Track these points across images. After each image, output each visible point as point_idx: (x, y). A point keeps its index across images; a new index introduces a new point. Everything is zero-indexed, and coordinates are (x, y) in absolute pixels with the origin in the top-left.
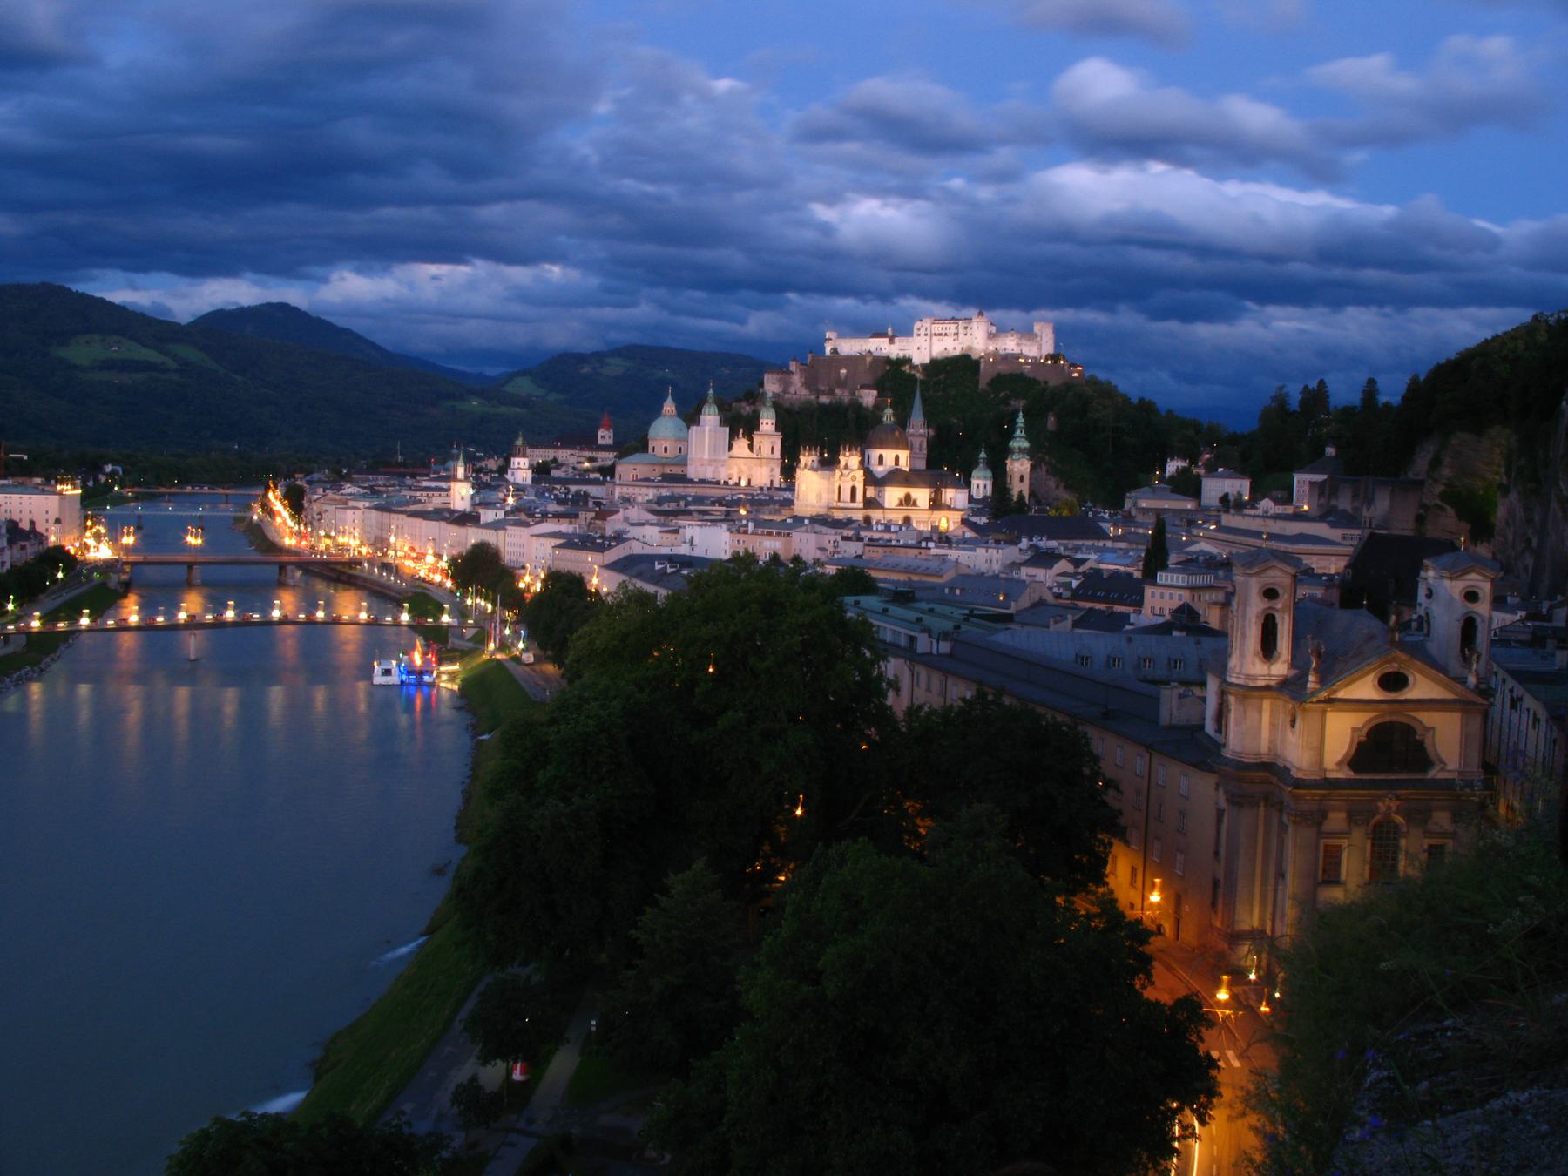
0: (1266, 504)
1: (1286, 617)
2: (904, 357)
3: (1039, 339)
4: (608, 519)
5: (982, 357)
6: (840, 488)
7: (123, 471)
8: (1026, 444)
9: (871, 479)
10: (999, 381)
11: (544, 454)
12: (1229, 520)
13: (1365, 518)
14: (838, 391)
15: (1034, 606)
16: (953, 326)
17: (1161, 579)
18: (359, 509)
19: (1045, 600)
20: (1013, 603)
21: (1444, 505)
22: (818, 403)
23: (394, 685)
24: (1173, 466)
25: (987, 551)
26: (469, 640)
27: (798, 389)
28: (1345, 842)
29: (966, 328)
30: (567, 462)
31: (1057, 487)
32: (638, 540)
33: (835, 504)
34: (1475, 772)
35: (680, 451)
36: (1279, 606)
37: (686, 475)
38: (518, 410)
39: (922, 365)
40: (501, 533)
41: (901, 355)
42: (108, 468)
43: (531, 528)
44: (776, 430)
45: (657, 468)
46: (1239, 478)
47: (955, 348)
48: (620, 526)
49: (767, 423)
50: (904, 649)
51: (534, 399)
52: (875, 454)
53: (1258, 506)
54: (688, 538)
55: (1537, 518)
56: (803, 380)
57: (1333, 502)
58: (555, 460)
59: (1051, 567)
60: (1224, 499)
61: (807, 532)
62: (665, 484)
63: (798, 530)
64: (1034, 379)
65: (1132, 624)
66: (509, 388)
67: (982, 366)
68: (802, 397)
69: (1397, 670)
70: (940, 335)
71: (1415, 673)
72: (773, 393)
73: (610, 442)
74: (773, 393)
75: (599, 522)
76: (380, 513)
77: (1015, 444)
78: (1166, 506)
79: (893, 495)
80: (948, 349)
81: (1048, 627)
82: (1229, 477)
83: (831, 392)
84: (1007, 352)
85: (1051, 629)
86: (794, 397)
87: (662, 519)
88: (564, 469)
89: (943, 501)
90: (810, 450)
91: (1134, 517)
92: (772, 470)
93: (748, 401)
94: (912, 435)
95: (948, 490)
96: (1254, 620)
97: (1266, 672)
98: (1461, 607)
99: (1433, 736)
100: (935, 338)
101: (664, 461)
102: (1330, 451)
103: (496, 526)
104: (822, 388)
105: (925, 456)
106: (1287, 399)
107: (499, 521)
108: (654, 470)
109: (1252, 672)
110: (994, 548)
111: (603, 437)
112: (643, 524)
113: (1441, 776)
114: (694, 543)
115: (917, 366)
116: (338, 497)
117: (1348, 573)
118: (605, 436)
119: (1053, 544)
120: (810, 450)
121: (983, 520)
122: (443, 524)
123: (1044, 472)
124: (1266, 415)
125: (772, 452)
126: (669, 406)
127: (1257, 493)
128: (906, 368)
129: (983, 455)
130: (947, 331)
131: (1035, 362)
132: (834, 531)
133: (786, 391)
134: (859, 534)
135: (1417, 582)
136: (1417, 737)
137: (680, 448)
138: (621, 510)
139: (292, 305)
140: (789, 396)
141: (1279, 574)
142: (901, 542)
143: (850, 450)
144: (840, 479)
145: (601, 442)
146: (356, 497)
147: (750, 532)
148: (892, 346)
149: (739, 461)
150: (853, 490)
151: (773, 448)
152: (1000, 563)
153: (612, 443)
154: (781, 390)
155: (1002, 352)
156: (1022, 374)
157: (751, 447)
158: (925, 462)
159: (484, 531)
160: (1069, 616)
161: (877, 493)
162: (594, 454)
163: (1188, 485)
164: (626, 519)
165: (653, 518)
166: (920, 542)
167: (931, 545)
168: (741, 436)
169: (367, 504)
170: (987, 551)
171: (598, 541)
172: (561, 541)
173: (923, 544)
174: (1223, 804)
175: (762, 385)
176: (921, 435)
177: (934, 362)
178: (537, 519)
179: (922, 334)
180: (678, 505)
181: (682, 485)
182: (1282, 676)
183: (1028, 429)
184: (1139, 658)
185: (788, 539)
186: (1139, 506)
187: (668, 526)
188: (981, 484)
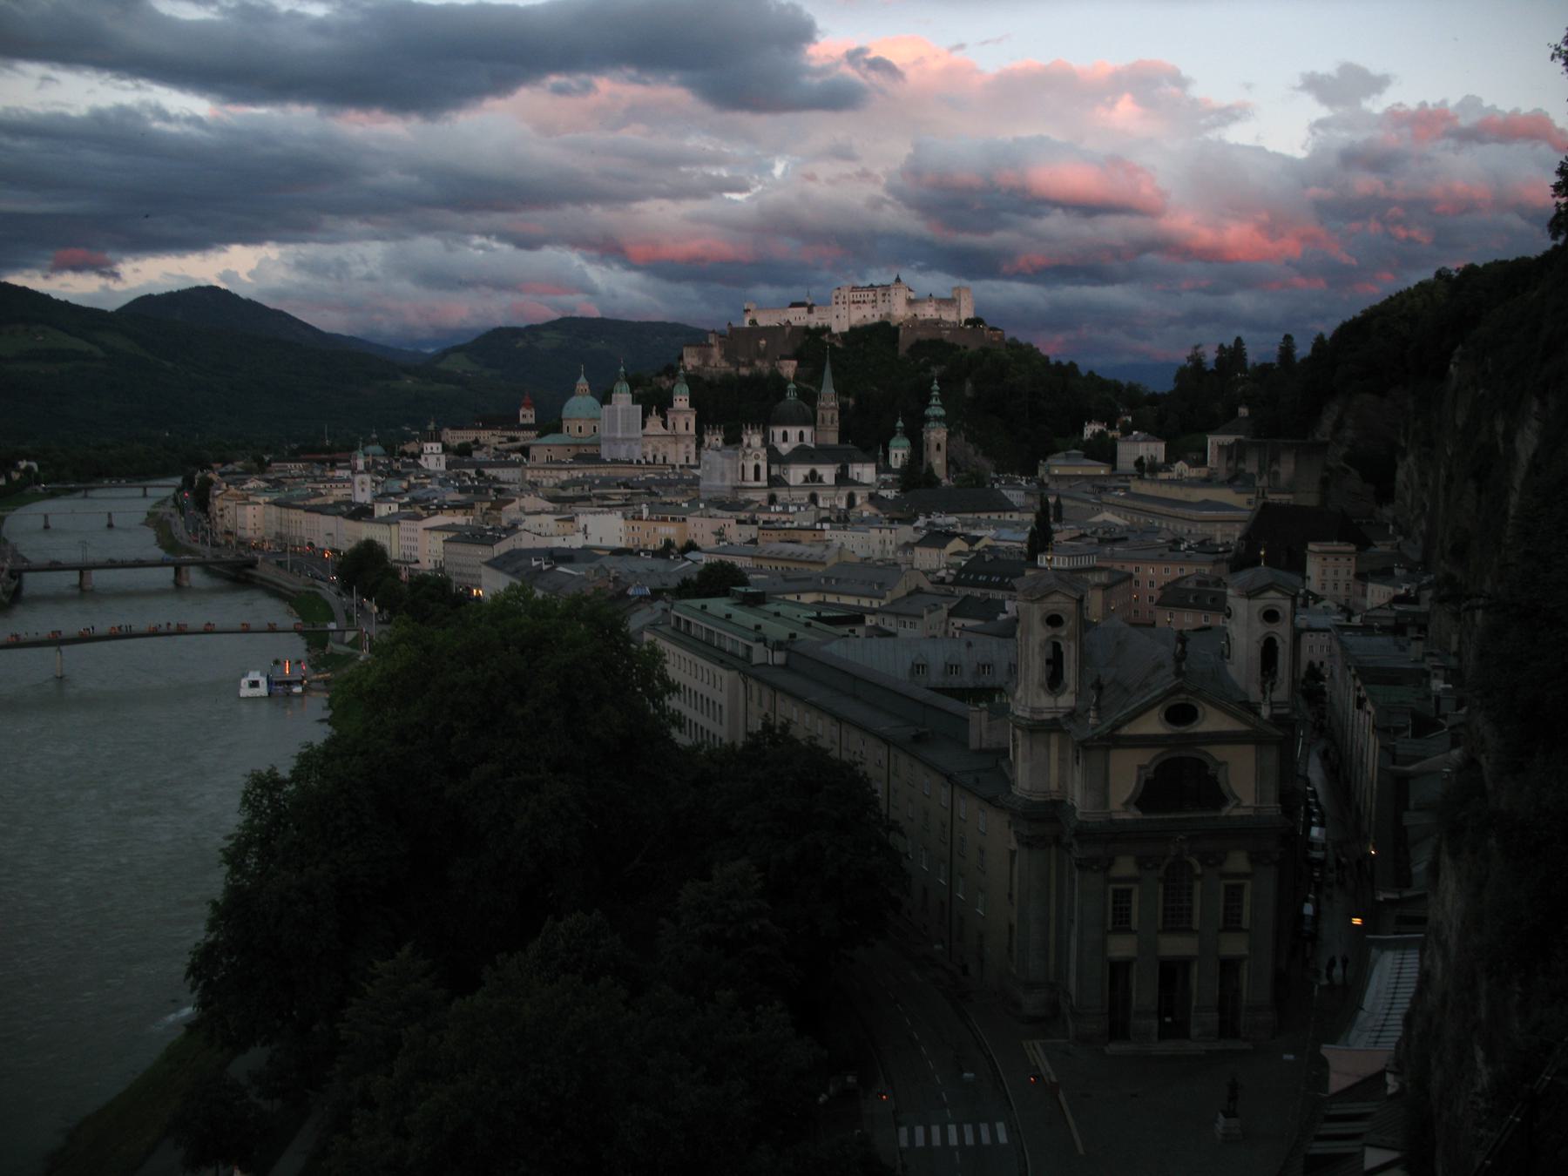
0: (1180, 466)
1: (1072, 644)
2: (823, 326)
3: (957, 304)
4: (504, 508)
5: (901, 324)
6: (743, 466)
7: (39, 467)
8: (942, 412)
9: (774, 456)
10: (918, 347)
11: (465, 436)
12: (1137, 486)
13: (1258, 487)
14: (758, 363)
15: (910, 594)
16: (871, 294)
17: (1041, 562)
18: (258, 504)
19: (922, 588)
20: (888, 593)
21: (1348, 467)
22: (738, 375)
23: (261, 697)
24: (1090, 430)
25: (880, 532)
26: (348, 644)
27: (718, 363)
29: (884, 295)
30: (488, 443)
31: (976, 453)
32: (529, 531)
33: (739, 484)
34: (1272, 808)
35: (595, 431)
36: (1064, 633)
37: (600, 455)
38: (453, 387)
39: (841, 333)
40: (394, 528)
41: (820, 324)
42: (23, 464)
43: (424, 521)
44: (690, 406)
45: (572, 449)
46: (1154, 441)
47: (874, 316)
48: (514, 516)
49: (682, 401)
50: (742, 659)
51: (470, 375)
52: (778, 431)
53: (1172, 469)
54: (581, 526)
55: (1430, 483)
56: (723, 352)
57: (1241, 466)
58: (476, 441)
59: (944, 546)
60: (1139, 463)
61: (702, 516)
62: (576, 466)
63: (692, 514)
64: (954, 345)
65: (1006, 612)
66: (443, 366)
67: (901, 332)
68: (722, 369)
69: (1184, 702)
70: (859, 302)
72: (693, 366)
73: (532, 420)
74: (693, 366)
75: (494, 512)
76: (278, 509)
77: (930, 413)
78: (1080, 473)
79: (797, 474)
80: (867, 316)
81: (922, 617)
82: (1144, 440)
83: (751, 364)
84: (926, 317)
85: (925, 618)
86: (714, 370)
87: (558, 506)
88: (485, 449)
89: (850, 476)
90: (714, 428)
91: (1047, 485)
92: (687, 446)
93: (668, 375)
94: (823, 408)
95: (855, 465)
96: (1037, 649)
97: (1053, 705)
98: (1261, 629)
100: (853, 306)
101: (578, 441)
102: (1243, 411)
103: (388, 521)
104: (742, 360)
105: (838, 429)
106: (1202, 358)
107: (393, 514)
108: (569, 450)
109: (1037, 705)
110: (887, 528)
111: (524, 416)
112: (538, 513)
113: (1236, 812)
114: (589, 530)
115: (836, 335)
116: (239, 493)
117: (1242, 545)
118: (527, 416)
119: (952, 519)
120: (714, 428)
121: (890, 494)
122: (340, 519)
123: (963, 439)
124: (1182, 374)
125: (687, 428)
126: (582, 383)
127: (1173, 456)
128: (826, 337)
129: (900, 424)
130: (866, 299)
131: (956, 328)
132: (729, 514)
133: (705, 363)
134: (754, 516)
135: (1305, 556)
136: (1209, 772)
137: (595, 428)
138: (517, 499)
139: (155, 294)
140: (709, 369)
141: (1062, 599)
142: (795, 525)
143: (752, 429)
144: (743, 458)
145: (522, 421)
146: (257, 491)
147: (644, 518)
148: (811, 316)
149: (653, 439)
150: (757, 468)
151: (687, 425)
152: (894, 543)
153: (534, 422)
154: (701, 363)
155: (921, 318)
156: (942, 340)
157: (665, 426)
158: (837, 434)
159: (379, 526)
160: (945, 606)
161: (782, 470)
162: (517, 434)
163: (1103, 451)
164: (522, 509)
165: (549, 506)
166: (815, 524)
167: (826, 526)
168: (654, 413)
169: (267, 499)
170: (880, 532)
171: (488, 533)
172: (451, 535)
173: (818, 526)
174: (1014, 845)
175: (681, 358)
176: (832, 408)
177: (853, 329)
178: (432, 512)
179: (840, 303)
180: (583, 489)
181: (594, 466)
182: (1069, 707)
183: (943, 396)
184: (978, 664)
185: (682, 524)
186: (1052, 473)
187: (564, 514)
188: (898, 453)
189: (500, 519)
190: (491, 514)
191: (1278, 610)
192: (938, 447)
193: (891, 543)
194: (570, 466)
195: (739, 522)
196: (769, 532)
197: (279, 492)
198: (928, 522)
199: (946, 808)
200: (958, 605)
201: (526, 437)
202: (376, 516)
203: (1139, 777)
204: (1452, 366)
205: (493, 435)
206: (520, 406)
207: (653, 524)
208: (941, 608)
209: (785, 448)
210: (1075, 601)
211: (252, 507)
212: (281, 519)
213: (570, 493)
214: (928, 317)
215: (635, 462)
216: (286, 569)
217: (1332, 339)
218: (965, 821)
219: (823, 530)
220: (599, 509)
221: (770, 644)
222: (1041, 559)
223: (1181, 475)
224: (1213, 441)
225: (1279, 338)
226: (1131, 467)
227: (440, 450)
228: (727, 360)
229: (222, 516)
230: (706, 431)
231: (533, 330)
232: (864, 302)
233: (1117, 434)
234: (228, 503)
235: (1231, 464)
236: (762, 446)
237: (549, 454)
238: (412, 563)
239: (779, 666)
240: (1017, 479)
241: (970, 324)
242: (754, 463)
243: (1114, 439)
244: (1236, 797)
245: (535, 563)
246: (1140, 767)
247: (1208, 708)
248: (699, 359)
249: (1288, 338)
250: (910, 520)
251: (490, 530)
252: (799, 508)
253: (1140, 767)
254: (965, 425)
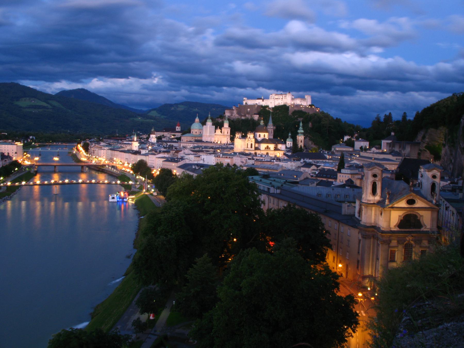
0: (374, 149)
2: (267, 105)
3: (307, 100)
6: (247, 144)
8: (303, 131)
9: (257, 141)
10: (295, 112)
12: (363, 154)
13: (403, 153)
14: (247, 115)
15: (305, 179)
16: (281, 96)
18: (105, 149)
20: (299, 178)
21: (426, 150)
22: (241, 119)
24: (346, 138)
25: (291, 163)
27: (235, 115)
28: (396, 249)
31: (312, 144)
32: (188, 159)
33: (246, 149)
36: (377, 179)
37: (202, 140)
38: (152, 120)
39: (272, 108)
40: (147, 157)
41: (266, 105)
42: (31, 137)
44: (229, 127)
45: (193, 138)
47: (282, 103)
48: (182, 155)
49: (226, 125)
50: (266, 192)
52: (258, 134)
53: (371, 150)
54: (202, 158)
55: (454, 154)
56: (237, 112)
57: (393, 149)
58: (163, 135)
60: (361, 148)
61: (238, 157)
62: (196, 143)
65: (334, 185)
70: (277, 99)
71: (418, 199)
72: (228, 116)
73: (180, 130)
74: (228, 116)
78: (344, 150)
79: (263, 146)
83: (245, 116)
85: (310, 186)
86: (234, 117)
87: (195, 153)
88: (166, 138)
90: (239, 133)
92: (227, 139)
93: (220, 118)
94: (269, 128)
97: (373, 199)
99: (423, 218)
100: (276, 100)
101: (196, 136)
102: (393, 134)
103: (146, 155)
104: (243, 114)
105: (273, 135)
107: (147, 153)
109: (369, 199)
111: (177, 129)
112: (189, 155)
114: (205, 160)
119: (311, 161)
120: (239, 133)
122: (130, 154)
123: (308, 140)
124: (374, 123)
125: (228, 133)
126: (197, 120)
127: (371, 146)
128: (267, 109)
129: (290, 134)
130: (279, 98)
131: (305, 107)
132: (246, 157)
133: (232, 115)
138: (183, 150)
141: (377, 170)
142: (266, 160)
143: (251, 133)
145: (177, 130)
146: (104, 146)
147: (221, 157)
150: (252, 145)
151: (228, 132)
154: (230, 115)
155: (296, 104)
157: (221, 132)
163: (350, 144)
164: (184, 153)
165: (192, 153)
166: (271, 160)
167: (274, 161)
168: (218, 128)
169: (108, 148)
170: (291, 163)
172: (165, 159)
173: (272, 161)
174: (360, 238)
175: (224, 113)
176: (272, 129)
177: (275, 107)
179: (272, 99)
180: (200, 149)
181: (201, 143)
182: (378, 200)
188: (289, 143)
189: (178, 156)
190: (175, 154)
191: (436, 175)
192: (301, 141)
193: (294, 166)
194: (194, 143)
195: (249, 159)
196: (258, 162)
197: (111, 146)
198: (304, 161)
199: (337, 230)
200: (319, 182)
201: (178, 135)
202: (141, 154)
203: (399, 219)
204: (462, 120)
205: (168, 134)
206: (176, 126)
207: (224, 159)
208: (314, 183)
209: (259, 139)
210: (381, 171)
211: (103, 150)
212: (112, 154)
213: (196, 149)
214: (298, 104)
215: (213, 142)
216: (115, 168)
217: (421, 113)
218: (343, 233)
219: (273, 162)
220: (206, 154)
221: (276, 187)
222: (342, 171)
223: (374, 152)
224: (384, 142)
225: (402, 113)
226: (359, 149)
227: (155, 137)
228: (238, 114)
229: (94, 153)
230: (236, 133)
231: (176, 105)
232: (279, 99)
233: (355, 139)
234: (95, 149)
235: (390, 148)
236: (253, 138)
237: (187, 139)
238: (152, 168)
239: (278, 194)
240: (325, 152)
241: (310, 106)
242: (251, 143)
243: (354, 141)
244: (425, 226)
245: (194, 167)
246: (399, 216)
248: (230, 114)
249: (405, 113)
250: (299, 160)
251: (176, 158)
252: (265, 156)
254: (309, 135)
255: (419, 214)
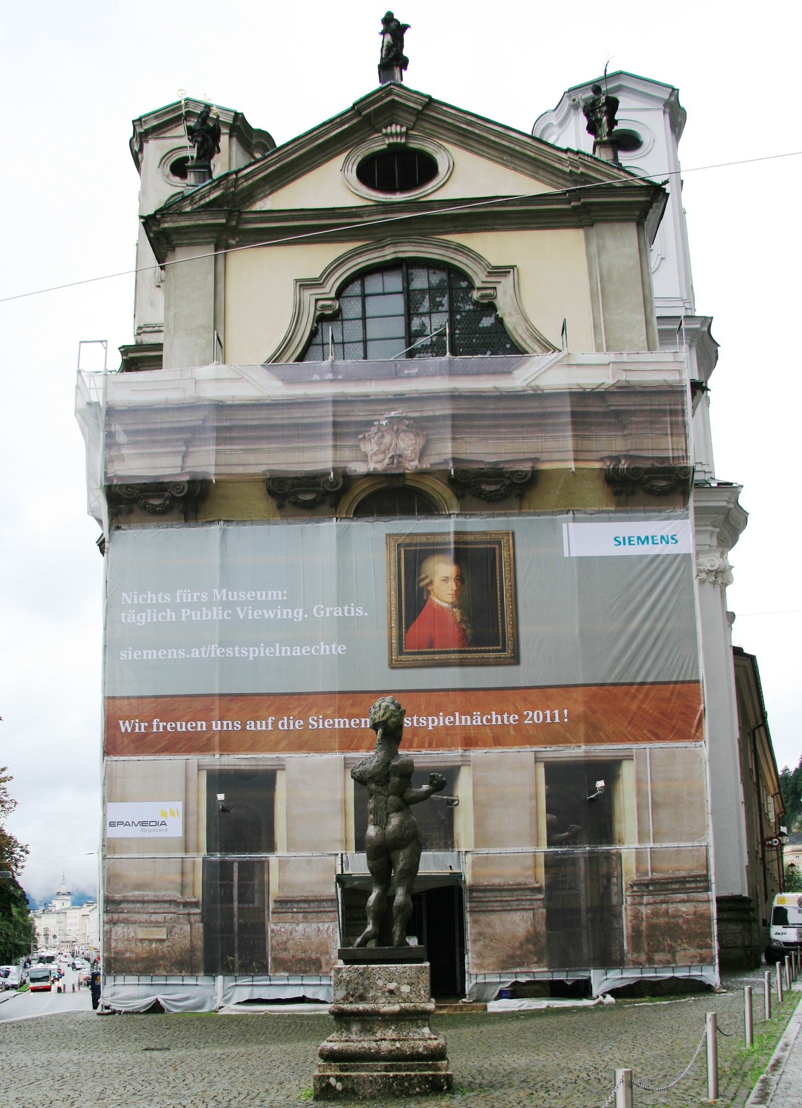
99: (516, 285)
247: (460, 155)
253: (304, 284)
255: (478, 258)
